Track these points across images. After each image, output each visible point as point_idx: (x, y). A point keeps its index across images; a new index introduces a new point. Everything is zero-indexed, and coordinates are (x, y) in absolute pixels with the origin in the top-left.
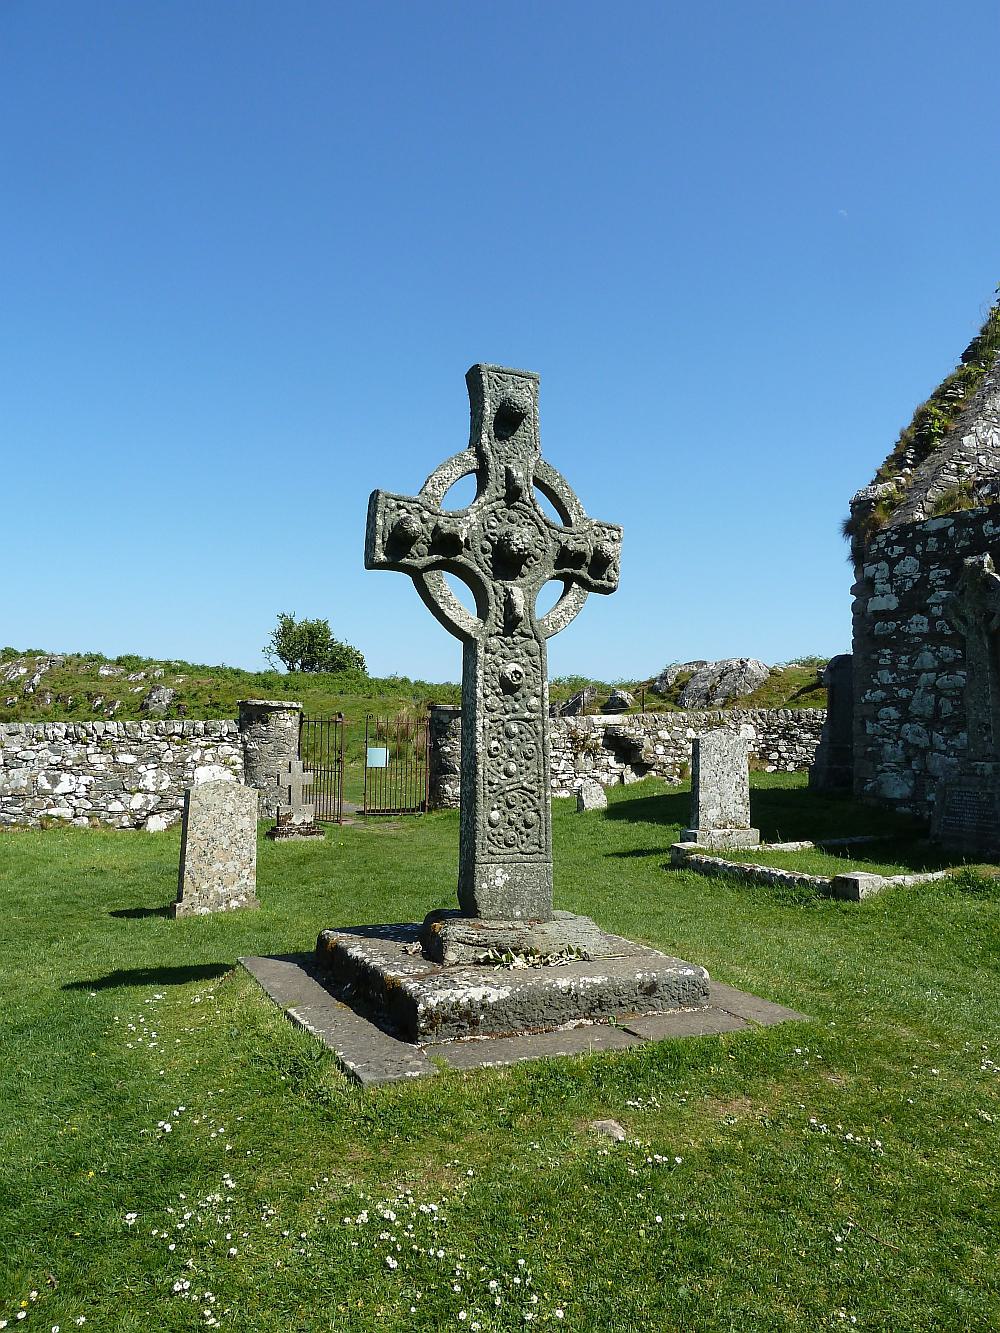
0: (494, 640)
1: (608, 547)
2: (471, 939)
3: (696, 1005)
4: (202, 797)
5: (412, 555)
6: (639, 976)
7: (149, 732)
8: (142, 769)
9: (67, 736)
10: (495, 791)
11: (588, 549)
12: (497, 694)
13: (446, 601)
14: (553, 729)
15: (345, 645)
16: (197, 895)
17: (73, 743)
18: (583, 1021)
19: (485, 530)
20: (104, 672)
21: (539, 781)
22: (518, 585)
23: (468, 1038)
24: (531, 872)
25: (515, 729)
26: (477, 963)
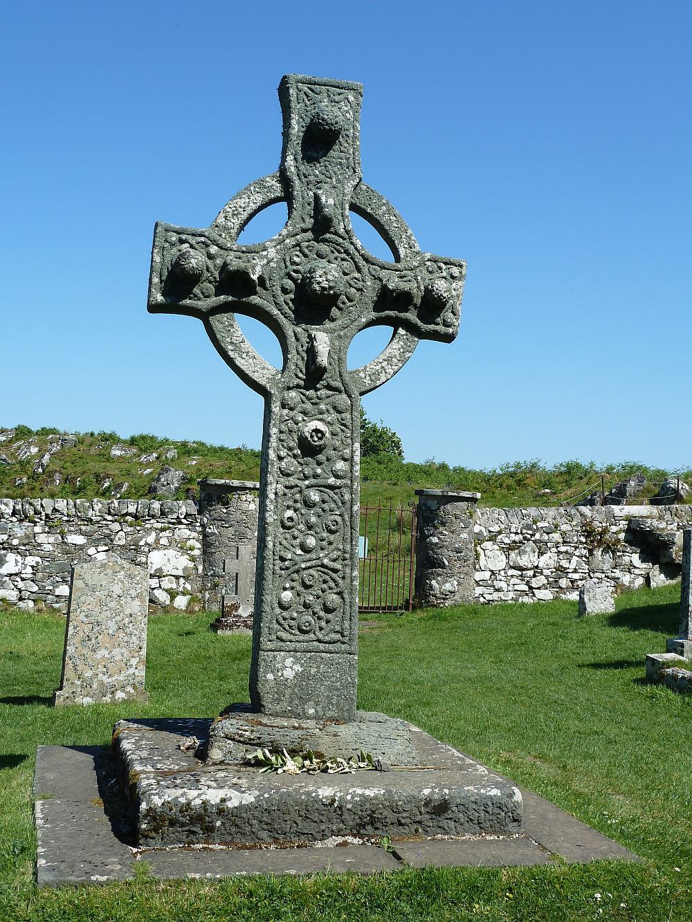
0: (293, 394)
1: (441, 286)
2: (241, 736)
3: (504, 832)
4: (87, 577)
5: (195, 296)
6: (426, 792)
7: (100, 511)
8: (92, 551)
9: (14, 514)
10: (287, 568)
11: (415, 289)
12: (295, 456)
13: (240, 353)
14: (564, 519)
15: (379, 426)
16: (79, 683)
17: (21, 521)
18: (350, 839)
19: (286, 267)
20: (116, 452)
21: (344, 559)
22: (325, 331)
23: (200, 846)
24: (330, 664)
25: (315, 496)
26: (247, 763)
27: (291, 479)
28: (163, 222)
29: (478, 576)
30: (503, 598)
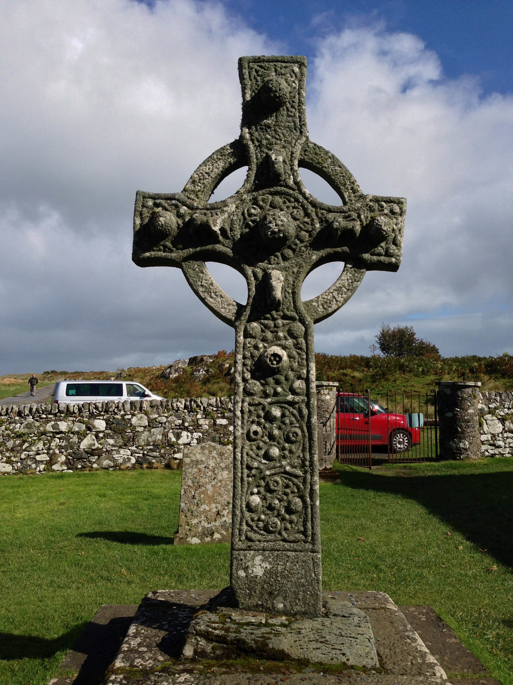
25: (277, 412)
27: (256, 398)
29: (483, 438)
30: (502, 452)
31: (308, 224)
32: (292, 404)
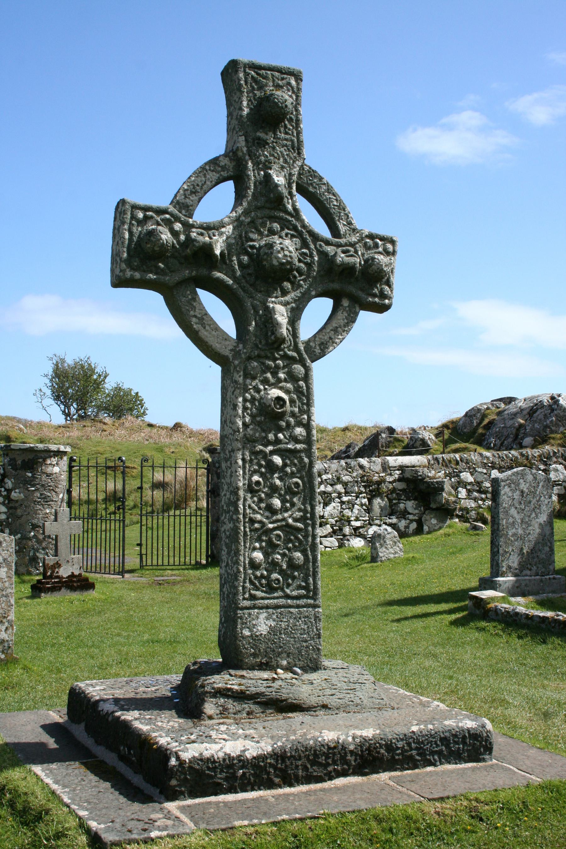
25: (277, 460)
28: (133, 199)
31: (307, 255)
32: (294, 452)
